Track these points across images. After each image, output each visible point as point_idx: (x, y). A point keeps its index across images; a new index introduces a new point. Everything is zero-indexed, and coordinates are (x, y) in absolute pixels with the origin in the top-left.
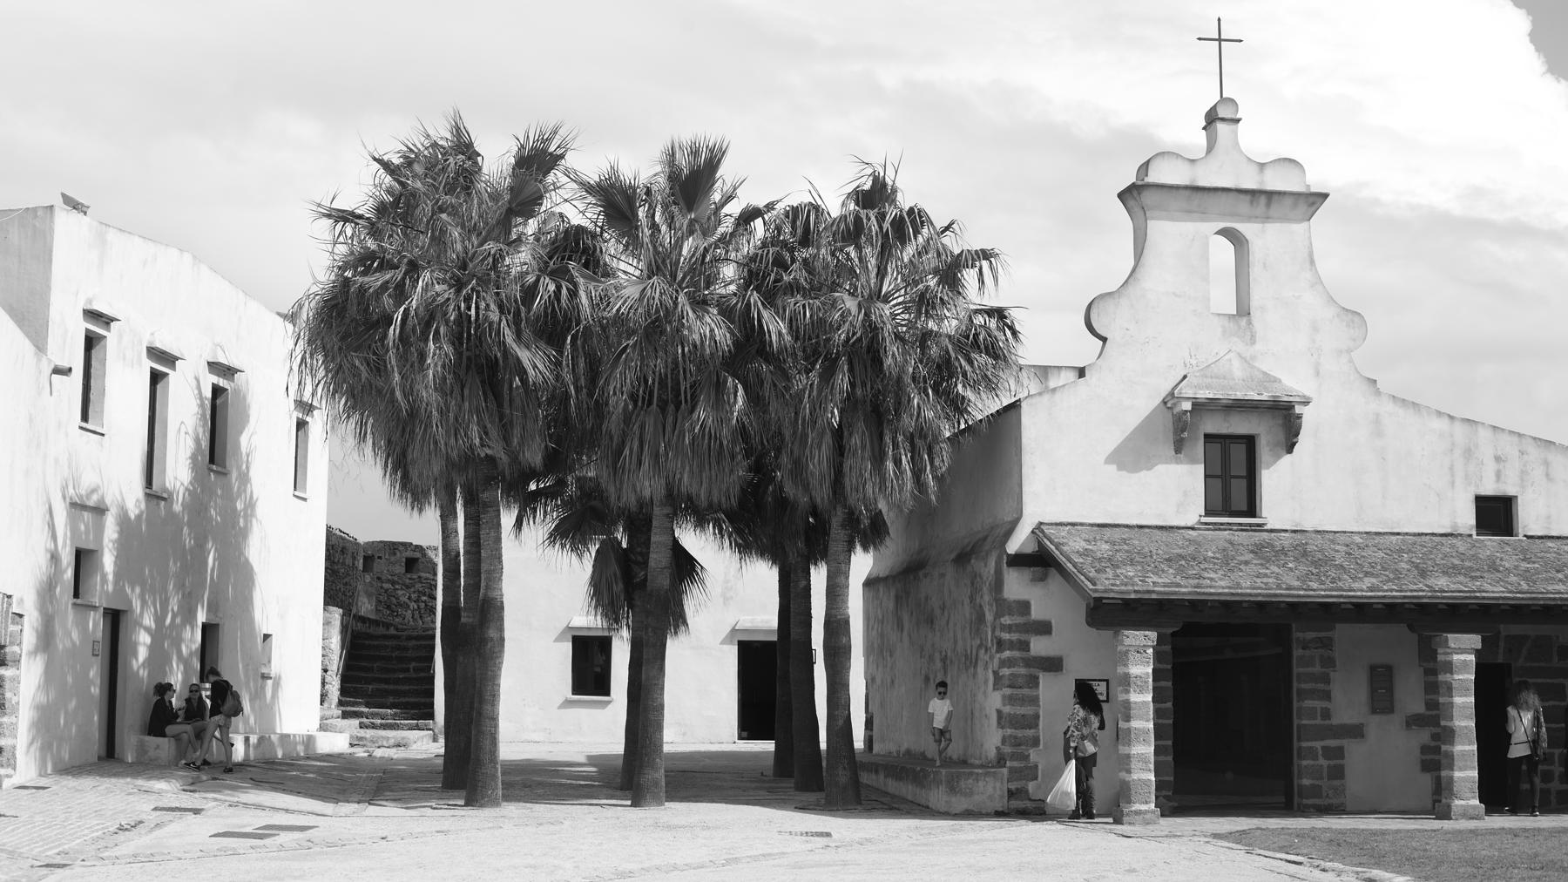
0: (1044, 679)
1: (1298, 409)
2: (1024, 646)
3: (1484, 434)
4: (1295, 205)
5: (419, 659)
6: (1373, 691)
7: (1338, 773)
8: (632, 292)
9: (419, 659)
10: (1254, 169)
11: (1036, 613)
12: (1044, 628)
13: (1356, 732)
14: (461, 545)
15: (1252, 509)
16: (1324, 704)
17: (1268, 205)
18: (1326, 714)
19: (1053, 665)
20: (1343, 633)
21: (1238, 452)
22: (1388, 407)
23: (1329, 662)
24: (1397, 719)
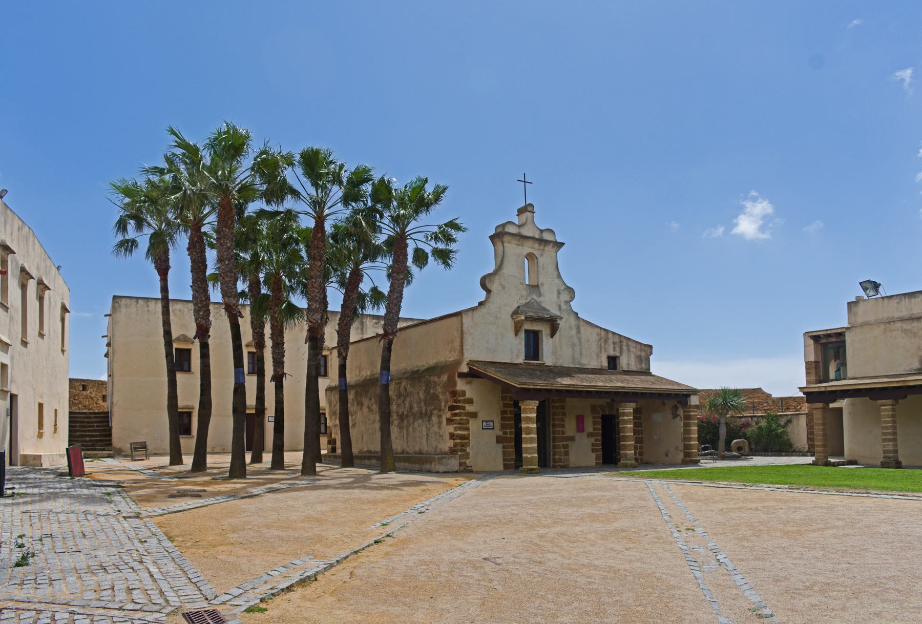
0: (471, 421)
1: (559, 321)
2: (464, 408)
3: (610, 335)
5: (75, 431)
6: (578, 424)
7: (567, 454)
8: (378, 242)
9: (75, 431)
11: (468, 395)
12: (470, 401)
13: (572, 439)
15: (110, 444)
18: (563, 433)
19: (474, 415)
20: (570, 401)
22: (582, 323)
23: (564, 414)
24: (585, 434)
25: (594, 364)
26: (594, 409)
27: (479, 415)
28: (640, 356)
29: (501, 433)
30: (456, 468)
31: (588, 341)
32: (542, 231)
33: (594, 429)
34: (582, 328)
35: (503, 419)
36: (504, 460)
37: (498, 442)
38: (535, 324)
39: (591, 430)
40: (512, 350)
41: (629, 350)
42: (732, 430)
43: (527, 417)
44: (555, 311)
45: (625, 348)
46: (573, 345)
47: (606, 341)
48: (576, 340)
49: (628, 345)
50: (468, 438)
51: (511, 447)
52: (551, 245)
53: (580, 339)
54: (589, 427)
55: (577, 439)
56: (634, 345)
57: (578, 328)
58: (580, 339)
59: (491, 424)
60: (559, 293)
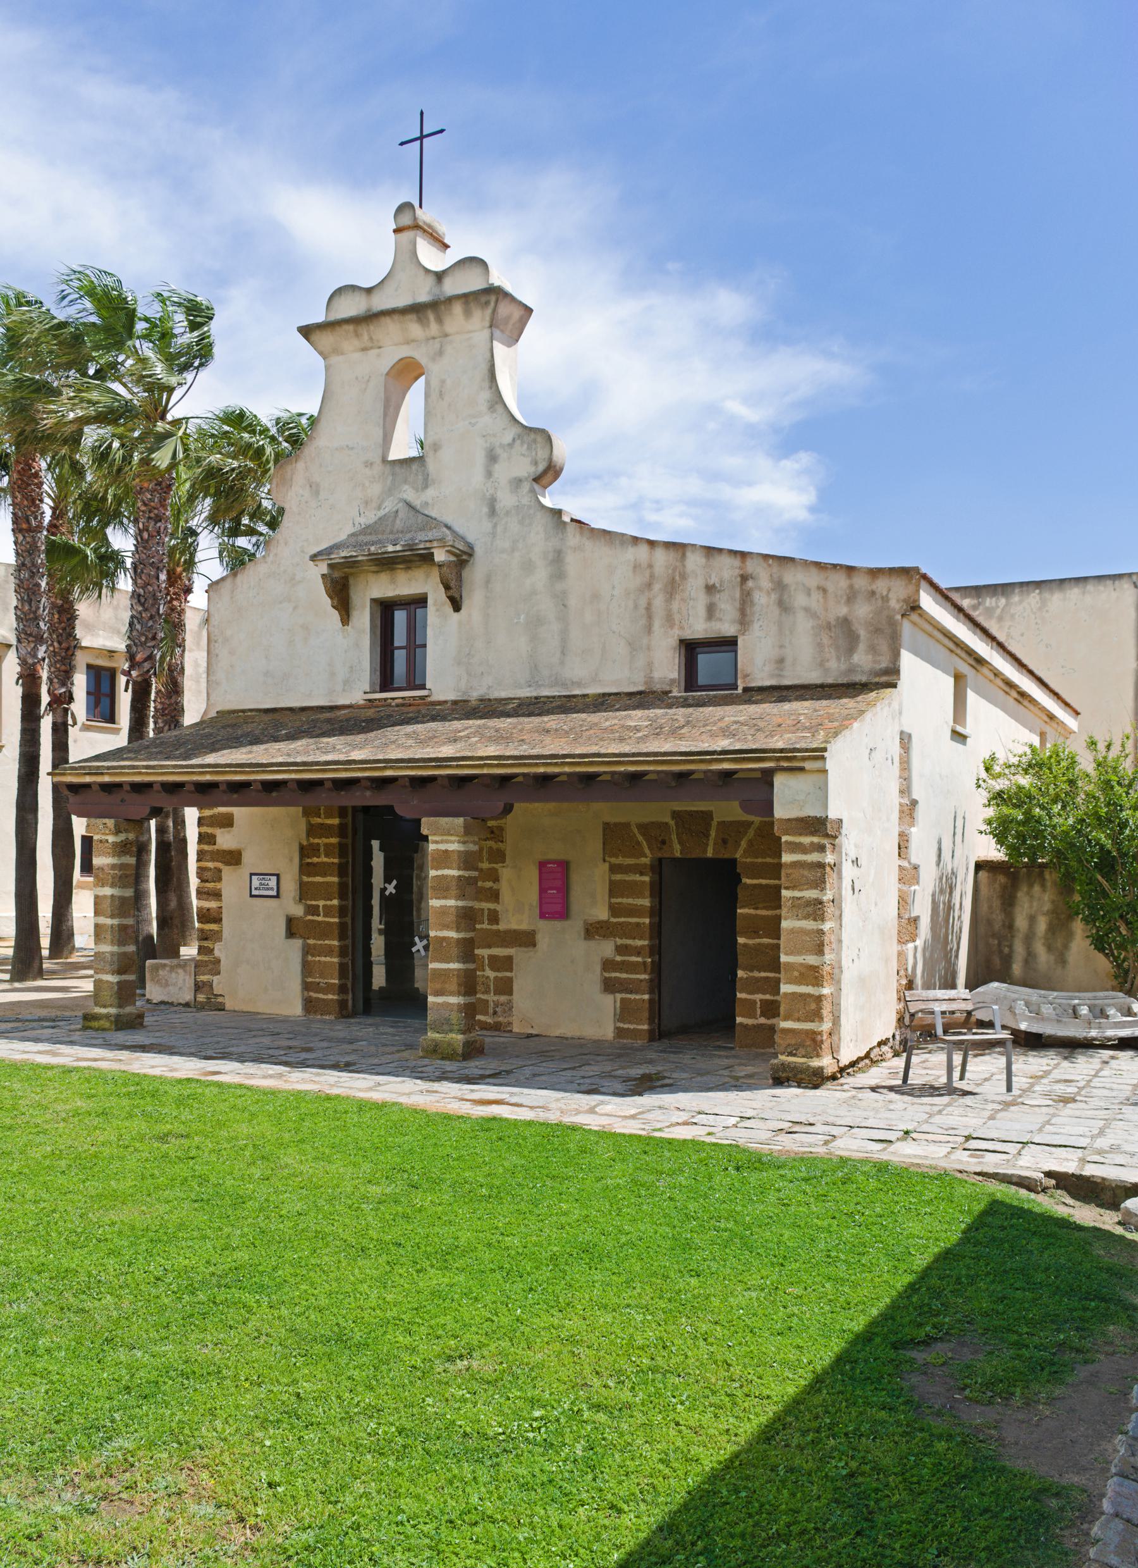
0: (227, 871)
3: (694, 561)
4: (468, 313)
7: (505, 987)
10: (431, 280)
13: (527, 939)
14: (624, 900)
16: (492, 906)
17: (440, 320)
18: (494, 918)
21: (105, 676)
22: (573, 537)
24: (573, 927)
25: (619, 677)
26: (615, 837)
27: (246, 858)
28: (845, 623)
29: (298, 911)
30: (187, 996)
31: (596, 597)
32: (439, 276)
33: (614, 910)
34: (572, 561)
35: (306, 868)
36: (306, 986)
37: (291, 933)
38: (402, 576)
39: (602, 913)
40: (333, 662)
41: (784, 607)
42: (660, 943)
43: (642, 874)
44: (472, 527)
45: (763, 599)
46: (536, 623)
47: (673, 587)
48: (546, 606)
49: (780, 586)
50: (218, 920)
51: (329, 951)
52: (458, 308)
53: (561, 600)
54: (592, 899)
55: (543, 940)
56: (813, 579)
57: (557, 560)
58: (561, 600)
59: (273, 882)
60: (492, 457)
